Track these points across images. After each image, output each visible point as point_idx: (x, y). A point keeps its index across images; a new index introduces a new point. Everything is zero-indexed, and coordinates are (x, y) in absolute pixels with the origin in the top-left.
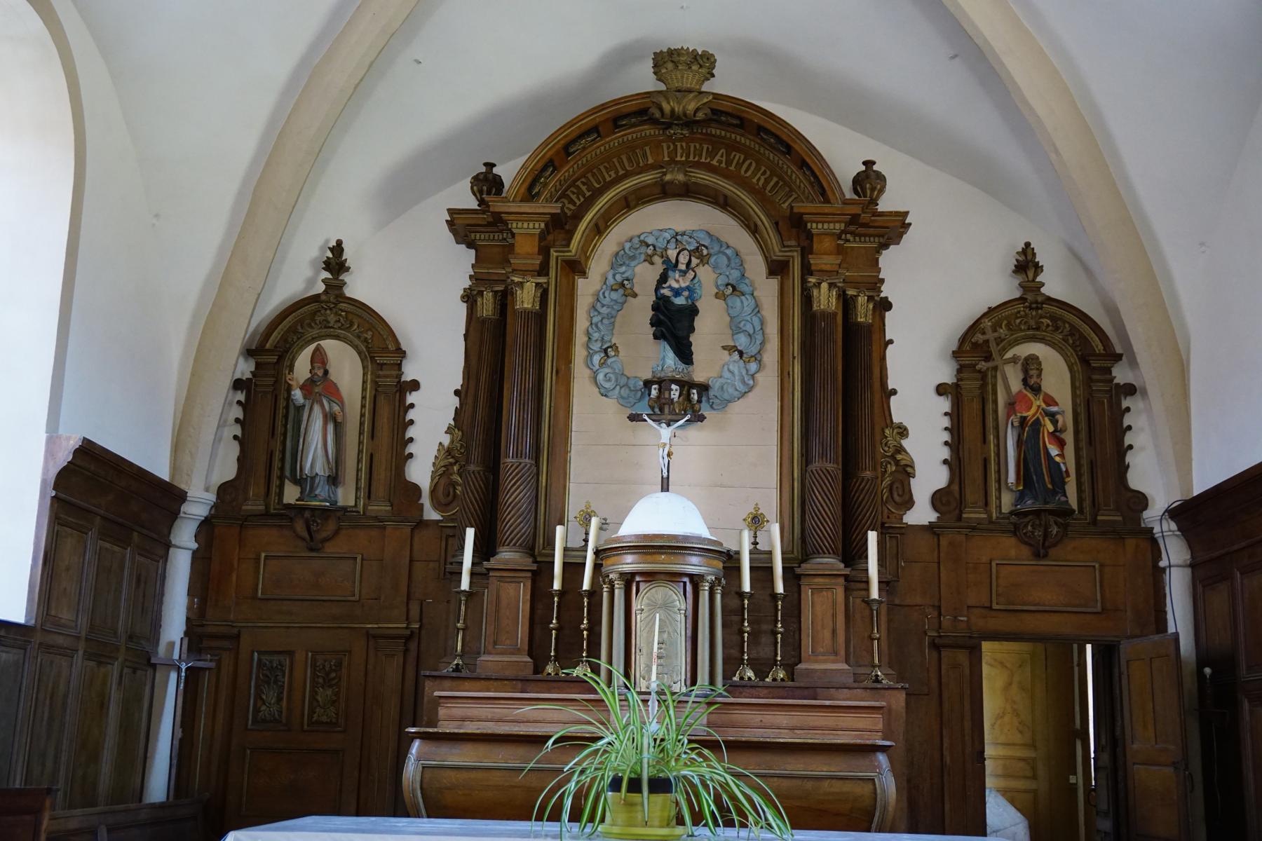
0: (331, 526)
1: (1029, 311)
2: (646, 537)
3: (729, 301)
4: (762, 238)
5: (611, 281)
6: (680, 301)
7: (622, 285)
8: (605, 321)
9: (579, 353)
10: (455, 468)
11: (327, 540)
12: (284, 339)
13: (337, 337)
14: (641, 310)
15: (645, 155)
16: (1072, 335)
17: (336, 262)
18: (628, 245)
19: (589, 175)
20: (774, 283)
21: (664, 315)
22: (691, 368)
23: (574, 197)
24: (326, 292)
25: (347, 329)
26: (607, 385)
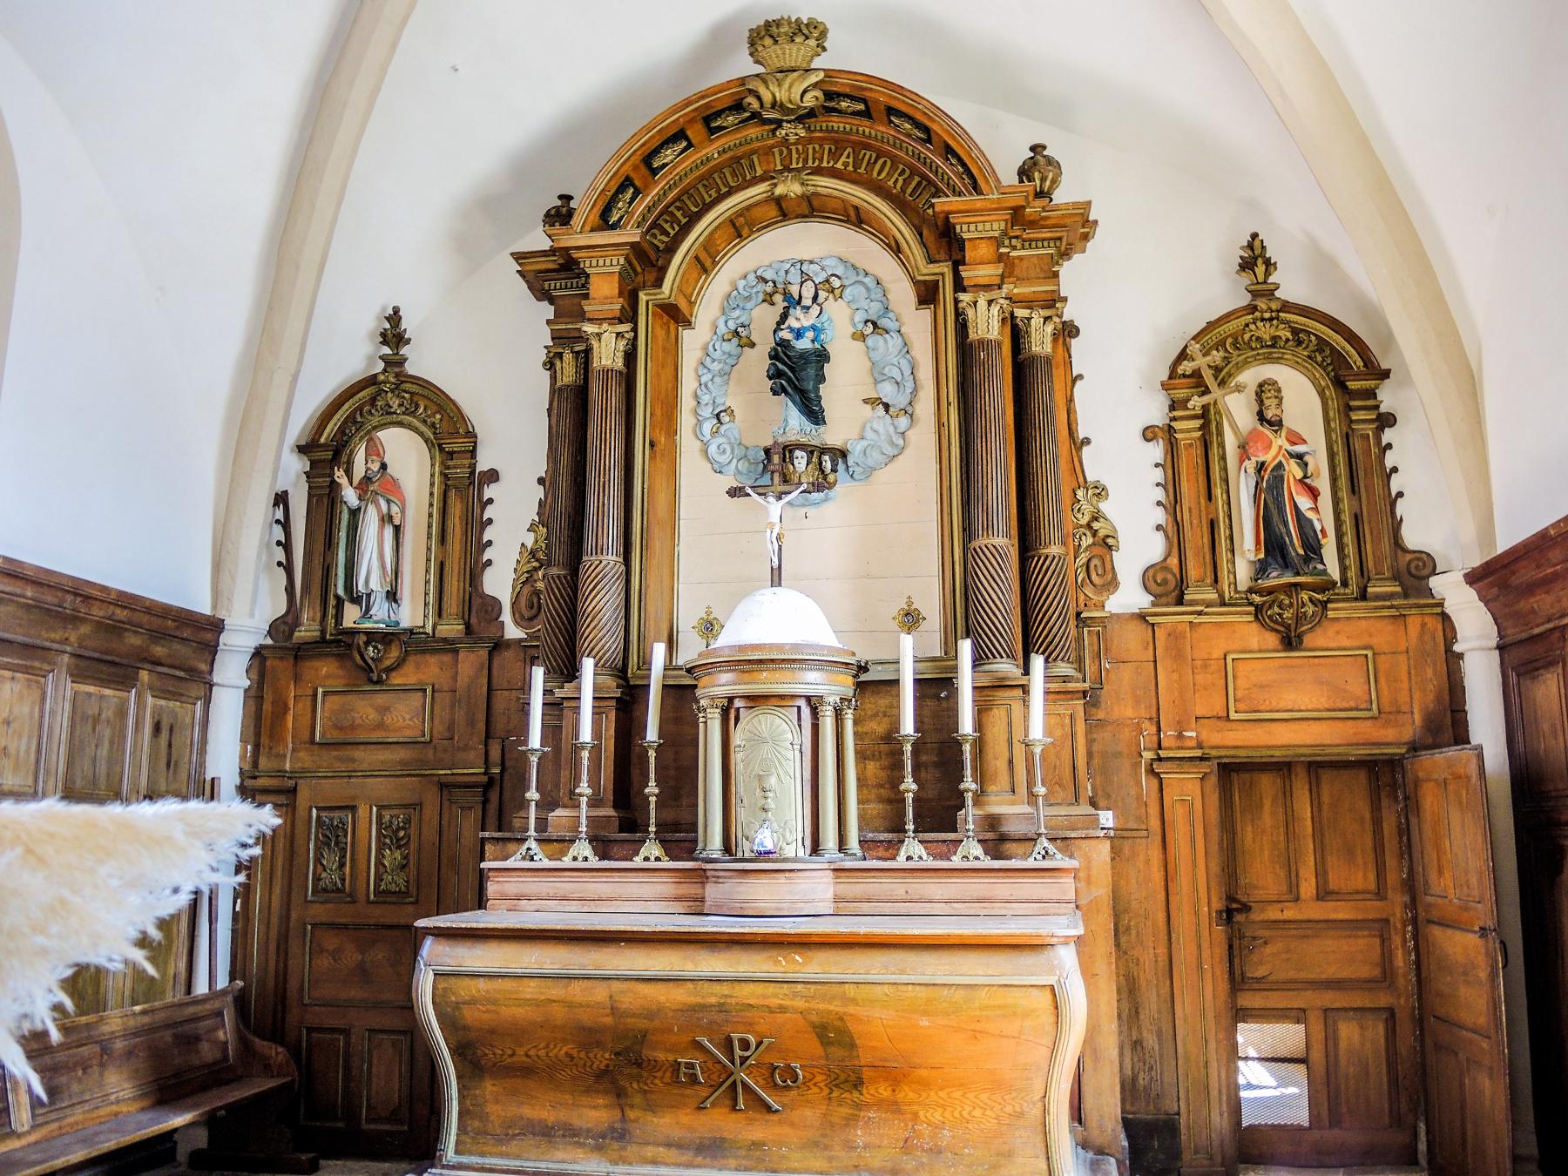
0: (394, 653)
1: (1267, 321)
2: (742, 648)
3: (870, 341)
4: (907, 258)
5: (722, 329)
6: (804, 344)
7: (736, 333)
8: (717, 380)
9: (686, 421)
10: (540, 573)
11: (389, 670)
12: (342, 430)
13: (400, 424)
14: (758, 361)
15: (752, 166)
16: (1320, 351)
17: (393, 335)
18: (741, 284)
19: (685, 198)
20: (926, 314)
21: (785, 364)
22: (822, 428)
23: (667, 226)
24: (385, 370)
25: (412, 414)
26: (723, 459)
